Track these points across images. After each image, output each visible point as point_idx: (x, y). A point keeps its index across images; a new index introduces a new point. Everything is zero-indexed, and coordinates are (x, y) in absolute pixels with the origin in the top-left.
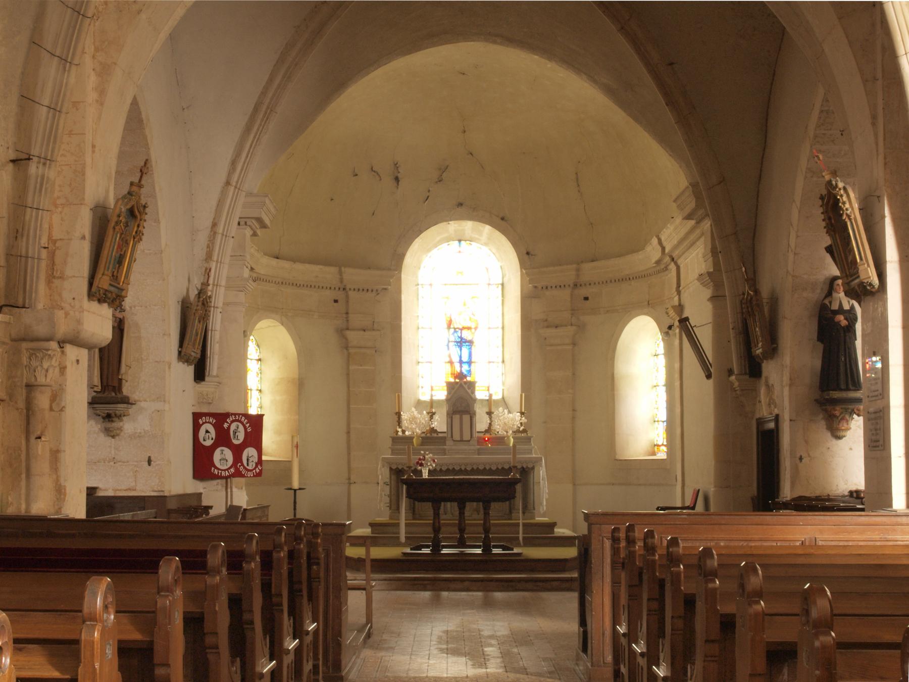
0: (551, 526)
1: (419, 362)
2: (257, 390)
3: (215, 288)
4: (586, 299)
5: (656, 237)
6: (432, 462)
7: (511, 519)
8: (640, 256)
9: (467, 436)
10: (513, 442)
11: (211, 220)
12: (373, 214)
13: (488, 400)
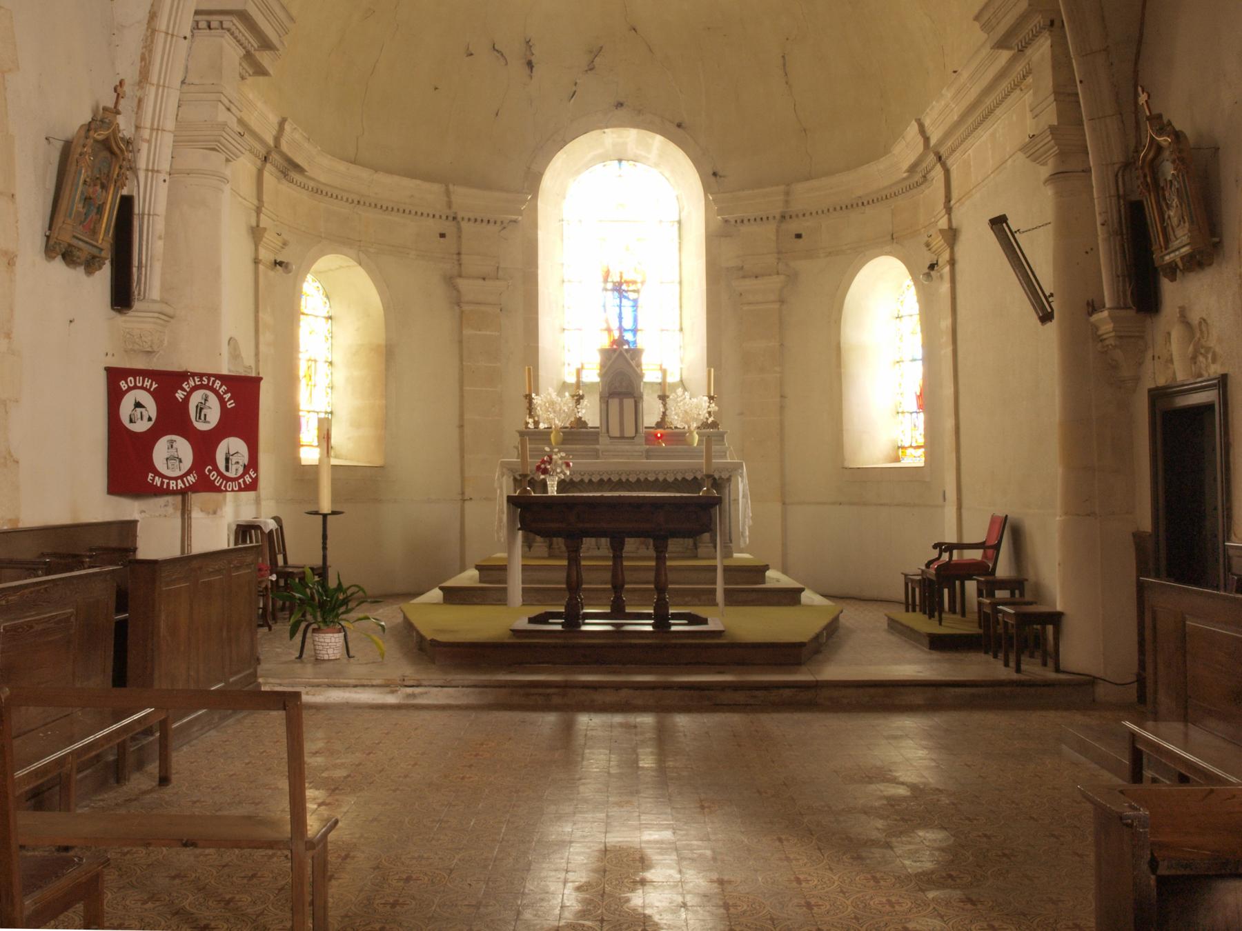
0: (759, 572)
1: (564, 329)
2: (326, 362)
3: (154, 134)
4: (799, 236)
5: (916, 120)
6: (564, 467)
7: (696, 557)
8: (882, 164)
9: (629, 431)
10: (698, 440)
11: (148, 8)
12: (497, 114)
13: (660, 384)
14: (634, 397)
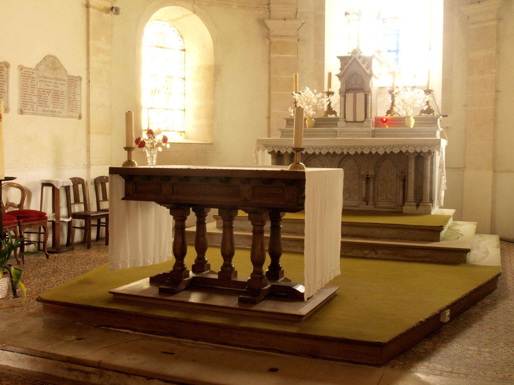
9: (360, 117)
14: (364, 91)
